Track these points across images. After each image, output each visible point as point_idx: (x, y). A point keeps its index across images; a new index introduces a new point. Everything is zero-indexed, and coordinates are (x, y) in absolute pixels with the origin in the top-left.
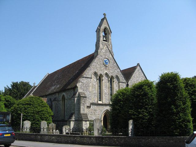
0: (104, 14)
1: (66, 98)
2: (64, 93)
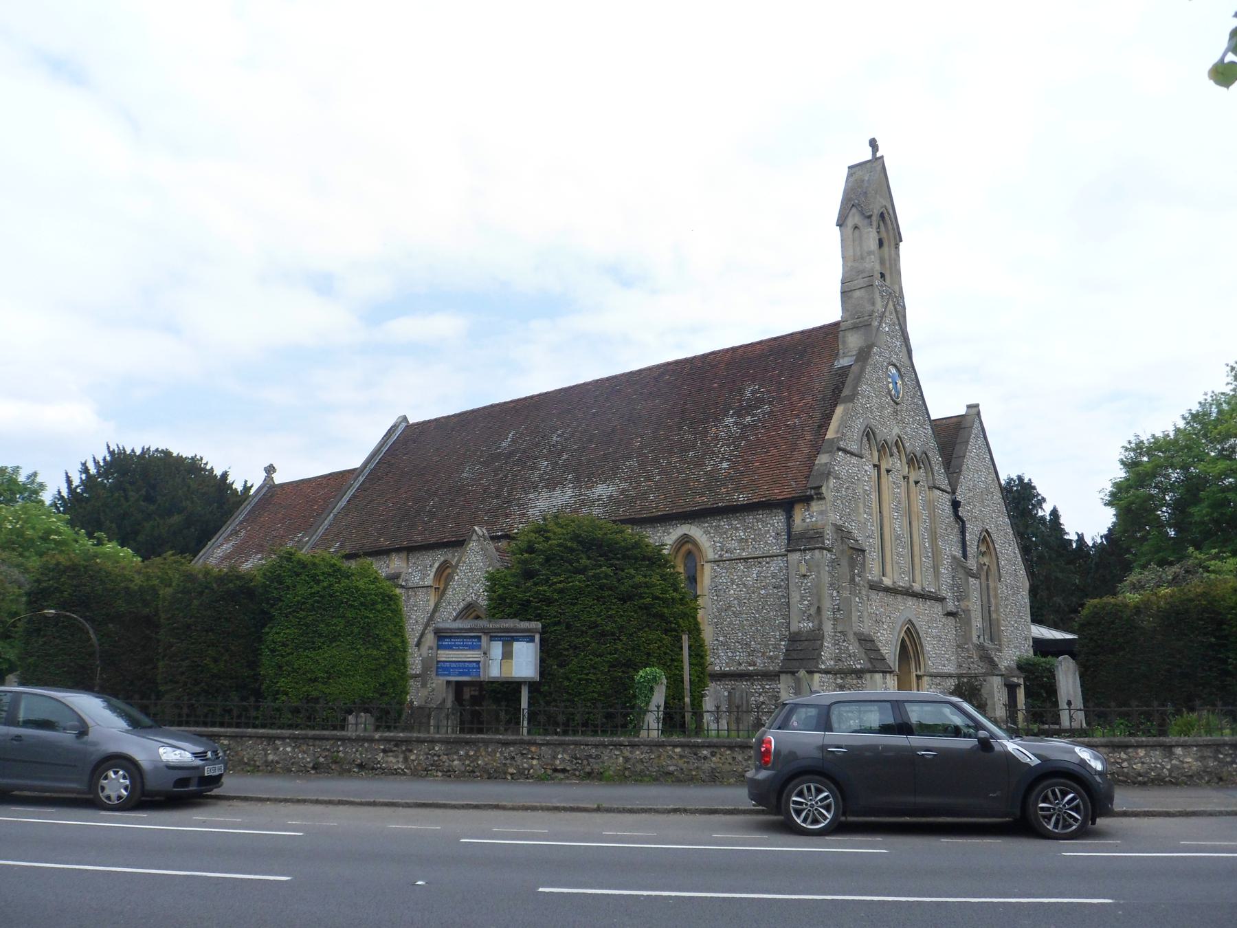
0: (873, 144)
2: (695, 531)
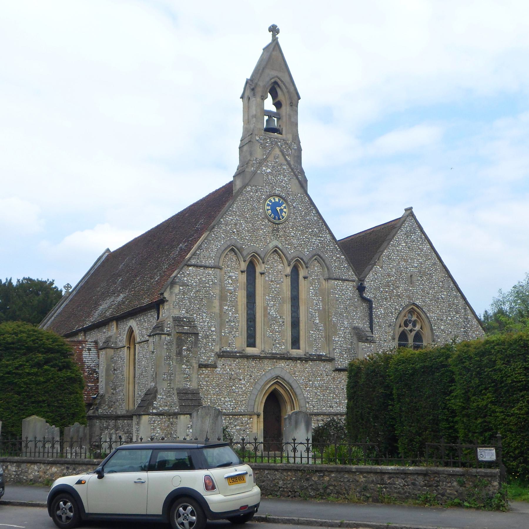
0: (274, 30)
1: (138, 340)
2: (132, 323)
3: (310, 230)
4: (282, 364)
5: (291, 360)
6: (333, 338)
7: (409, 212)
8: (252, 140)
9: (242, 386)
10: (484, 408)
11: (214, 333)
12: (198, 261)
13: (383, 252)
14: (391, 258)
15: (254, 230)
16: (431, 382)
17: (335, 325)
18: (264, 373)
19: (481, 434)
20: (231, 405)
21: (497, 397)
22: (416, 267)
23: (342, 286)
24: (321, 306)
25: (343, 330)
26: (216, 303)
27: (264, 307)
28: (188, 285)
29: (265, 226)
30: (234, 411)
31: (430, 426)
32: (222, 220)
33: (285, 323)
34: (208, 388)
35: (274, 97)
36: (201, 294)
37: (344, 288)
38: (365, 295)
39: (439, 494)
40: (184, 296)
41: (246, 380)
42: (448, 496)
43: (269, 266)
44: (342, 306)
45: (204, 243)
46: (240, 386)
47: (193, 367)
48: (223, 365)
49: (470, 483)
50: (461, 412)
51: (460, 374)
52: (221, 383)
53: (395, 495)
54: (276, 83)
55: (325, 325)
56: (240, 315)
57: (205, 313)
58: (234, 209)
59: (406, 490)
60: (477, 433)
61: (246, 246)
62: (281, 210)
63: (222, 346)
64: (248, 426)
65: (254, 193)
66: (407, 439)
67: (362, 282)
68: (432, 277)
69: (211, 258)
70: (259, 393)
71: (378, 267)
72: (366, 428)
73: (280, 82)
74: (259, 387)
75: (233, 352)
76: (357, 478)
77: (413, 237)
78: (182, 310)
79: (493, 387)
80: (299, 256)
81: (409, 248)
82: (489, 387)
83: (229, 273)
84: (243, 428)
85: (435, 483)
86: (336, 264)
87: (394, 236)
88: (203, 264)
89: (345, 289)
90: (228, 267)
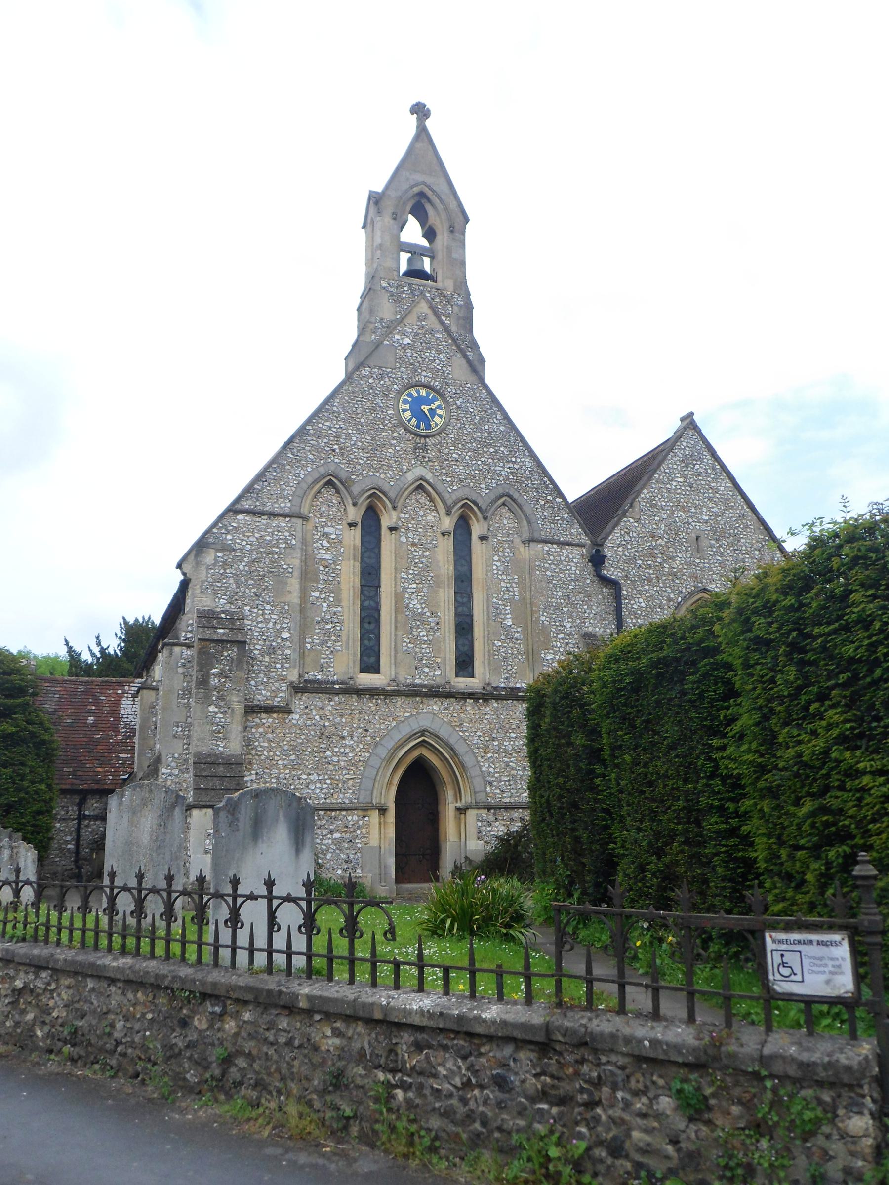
0: (420, 111)
3: (492, 450)
4: (435, 706)
5: (453, 697)
6: (543, 655)
7: (688, 421)
8: (373, 287)
9: (347, 750)
10: (817, 764)
11: (288, 643)
12: (258, 504)
13: (639, 492)
14: (656, 505)
15: (376, 448)
16: (676, 701)
17: (545, 630)
18: (394, 724)
19: (816, 851)
20: (321, 789)
21: (860, 720)
22: (706, 522)
23: (560, 556)
24: (516, 594)
25: (562, 639)
26: (294, 584)
27: (396, 594)
28: (234, 550)
29: (399, 439)
30: (328, 801)
31: (680, 827)
32: (310, 427)
33: (442, 624)
34: (271, 754)
35: (422, 218)
36: (261, 568)
37: (563, 558)
38: (605, 572)
39: (600, 1143)
40: (225, 569)
41: (355, 738)
42: (638, 1158)
43: (407, 516)
44: (560, 594)
45: (271, 469)
46: (342, 750)
47: (233, 710)
48: (306, 707)
49: (736, 1110)
50: (754, 783)
51: (747, 665)
52: (302, 743)
53: (435, 1123)
54: (421, 194)
55: (525, 629)
56: (346, 610)
57: (268, 603)
58: (335, 409)
59: (472, 1105)
60: (802, 848)
61: (357, 476)
62: (433, 412)
63: (306, 670)
64: (358, 832)
65: (377, 381)
66: (633, 863)
67: (600, 548)
68: (739, 541)
69: (285, 498)
70: (384, 764)
71: (632, 520)
72: (558, 835)
73: (429, 193)
74: (383, 752)
75: (328, 682)
76: (316, 1038)
77: (697, 466)
78: (221, 598)
79: (844, 686)
80: (469, 497)
81: (691, 487)
82: (833, 688)
83: (323, 527)
84: (348, 836)
85: (582, 1090)
86: (545, 514)
87: (659, 465)
88: (267, 508)
89: (564, 561)
90: (322, 517)
